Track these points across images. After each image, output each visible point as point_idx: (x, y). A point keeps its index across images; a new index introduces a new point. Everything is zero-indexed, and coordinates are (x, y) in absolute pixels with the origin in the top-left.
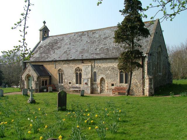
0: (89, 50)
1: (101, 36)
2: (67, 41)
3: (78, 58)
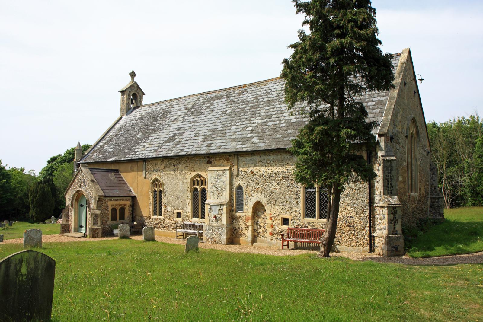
0: (228, 131)
1: (259, 98)
2: (177, 111)
3: (198, 152)
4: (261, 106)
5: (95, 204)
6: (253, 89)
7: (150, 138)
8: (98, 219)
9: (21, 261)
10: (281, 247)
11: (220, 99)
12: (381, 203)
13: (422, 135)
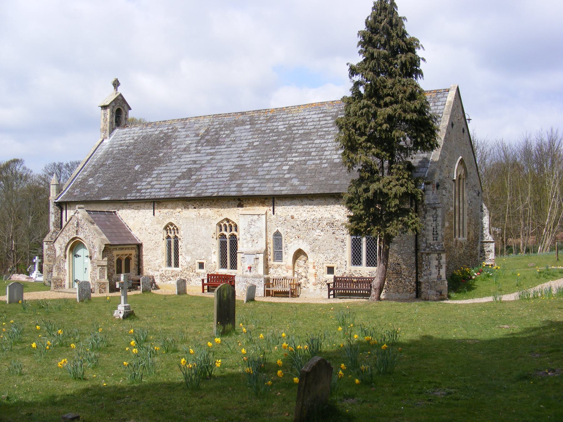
1: (293, 128)
3: (227, 194)
4: (296, 140)
5: (100, 254)
6: (283, 116)
7: (155, 172)
8: (104, 271)
9: (224, 290)
10: (327, 297)
11: (242, 125)
12: (427, 249)
13: (472, 175)
